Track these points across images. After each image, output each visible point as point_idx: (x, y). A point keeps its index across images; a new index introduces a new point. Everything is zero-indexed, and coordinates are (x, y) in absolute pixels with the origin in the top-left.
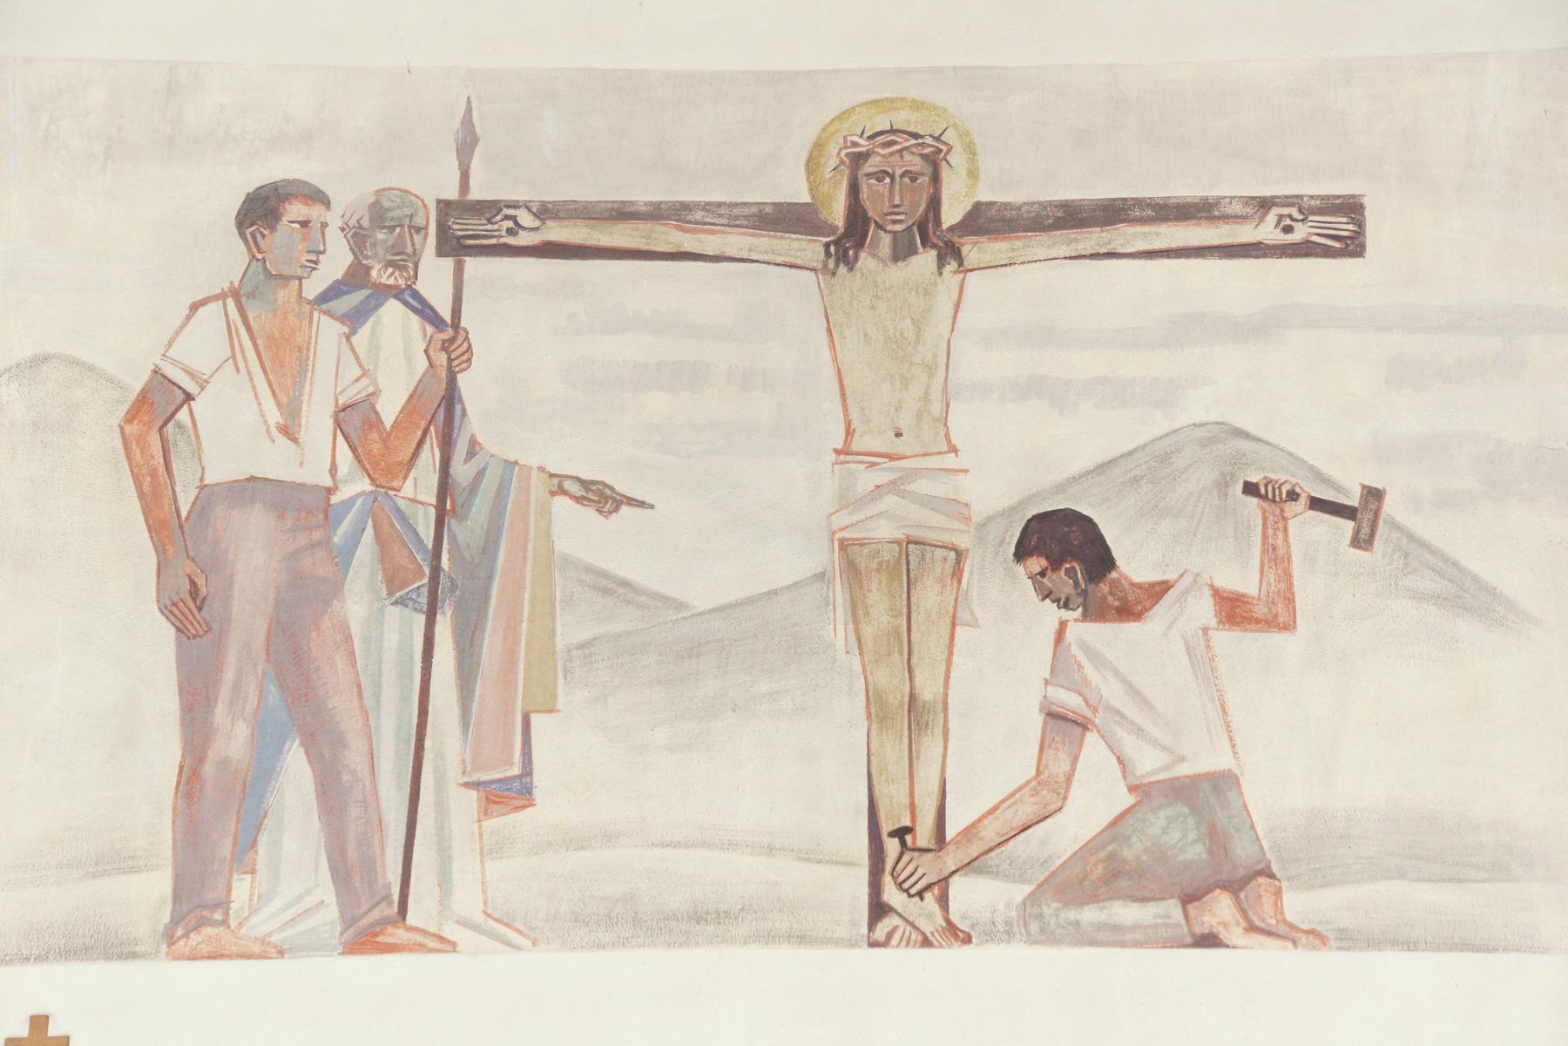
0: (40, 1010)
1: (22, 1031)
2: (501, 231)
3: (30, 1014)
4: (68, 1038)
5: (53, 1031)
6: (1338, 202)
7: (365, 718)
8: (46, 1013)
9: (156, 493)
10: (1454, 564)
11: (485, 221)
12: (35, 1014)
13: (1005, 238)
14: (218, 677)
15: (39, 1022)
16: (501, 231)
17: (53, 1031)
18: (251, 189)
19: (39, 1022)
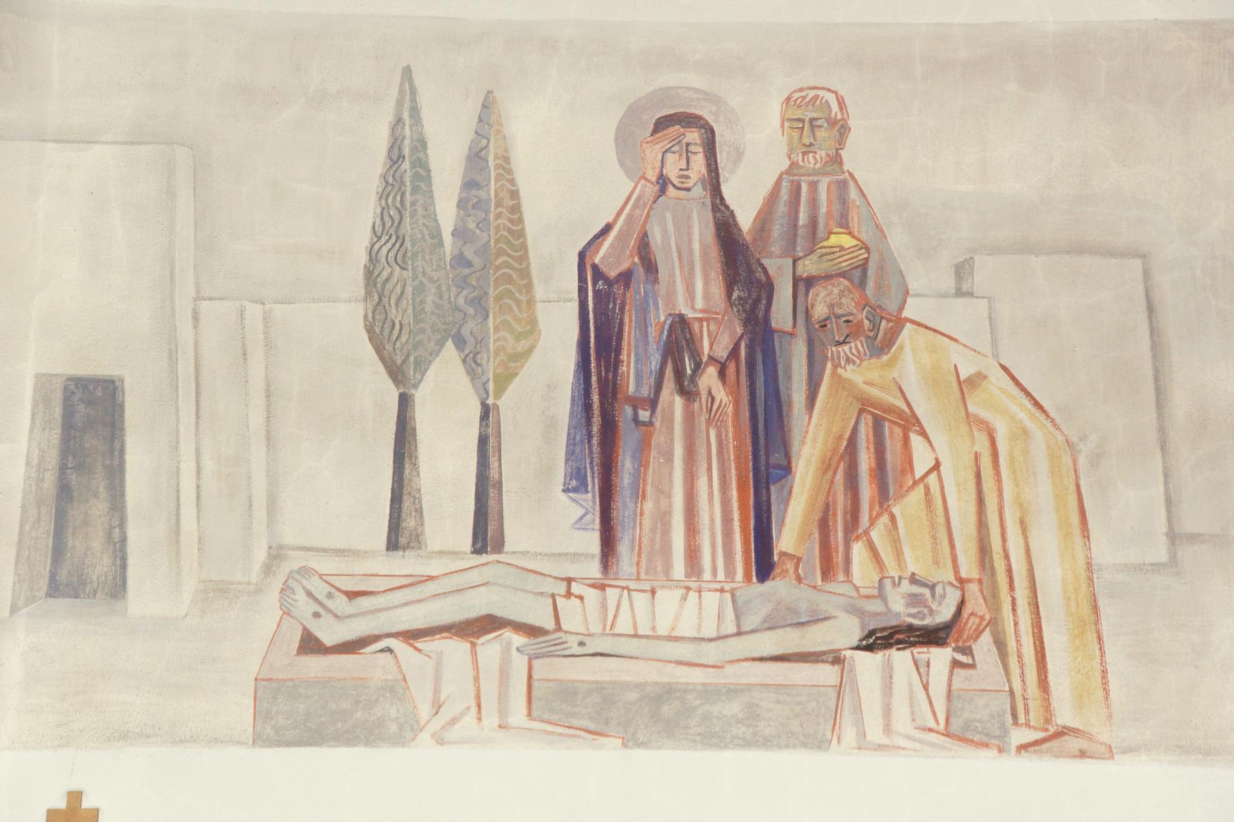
0: (74, 787)
1: (62, 804)
2: (790, 127)
3: (66, 789)
4: (98, 810)
5: (86, 804)
6: (638, 332)
7: (198, 363)
8: (80, 790)
9: (607, 385)
10: (1016, 480)
11: (801, 104)
12: (70, 790)
13: (579, 379)
14: (610, 250)
15: (75, 797)
16: (790, 127)
17: (86, 804)
18: (505, 544)
19: (75, 797)
